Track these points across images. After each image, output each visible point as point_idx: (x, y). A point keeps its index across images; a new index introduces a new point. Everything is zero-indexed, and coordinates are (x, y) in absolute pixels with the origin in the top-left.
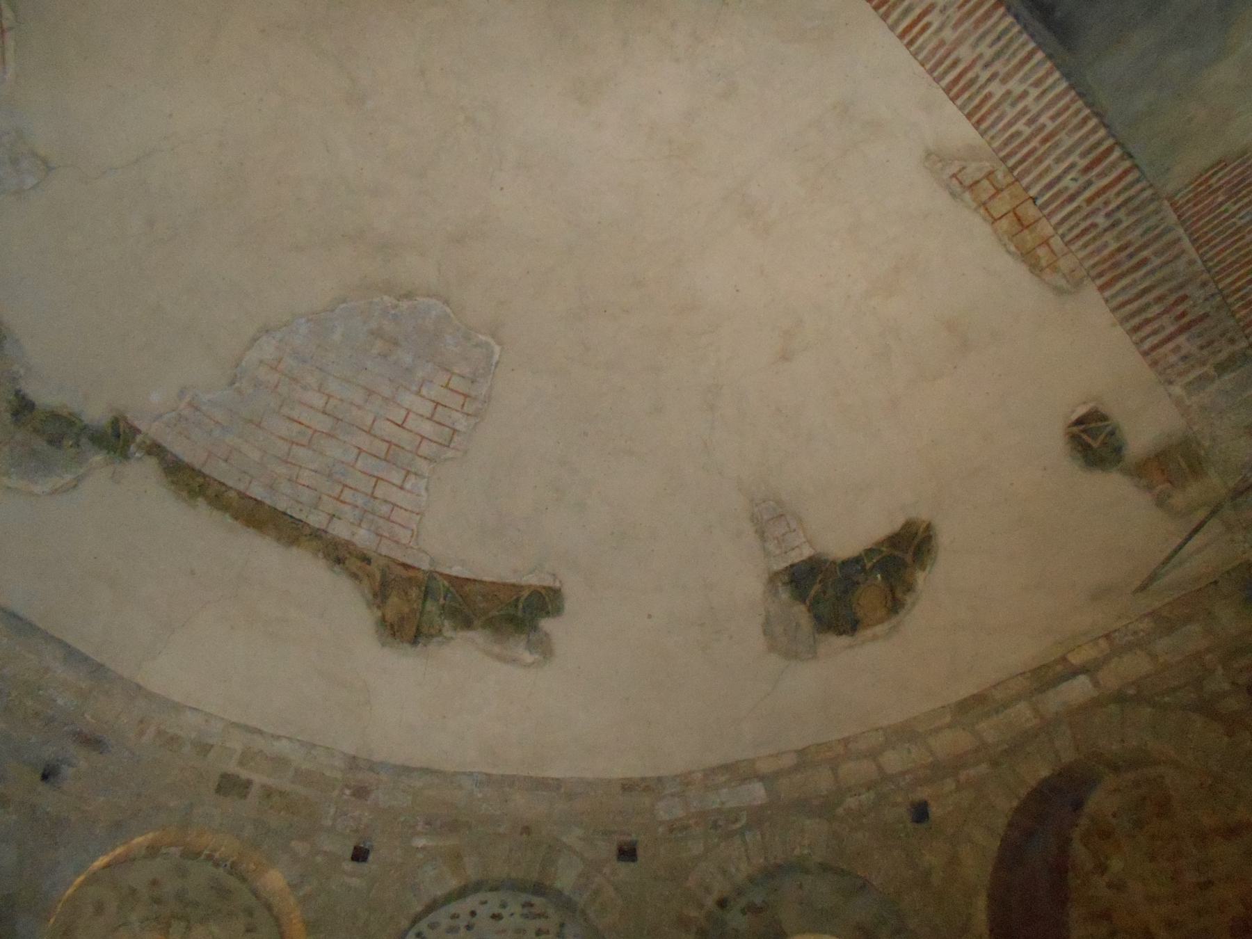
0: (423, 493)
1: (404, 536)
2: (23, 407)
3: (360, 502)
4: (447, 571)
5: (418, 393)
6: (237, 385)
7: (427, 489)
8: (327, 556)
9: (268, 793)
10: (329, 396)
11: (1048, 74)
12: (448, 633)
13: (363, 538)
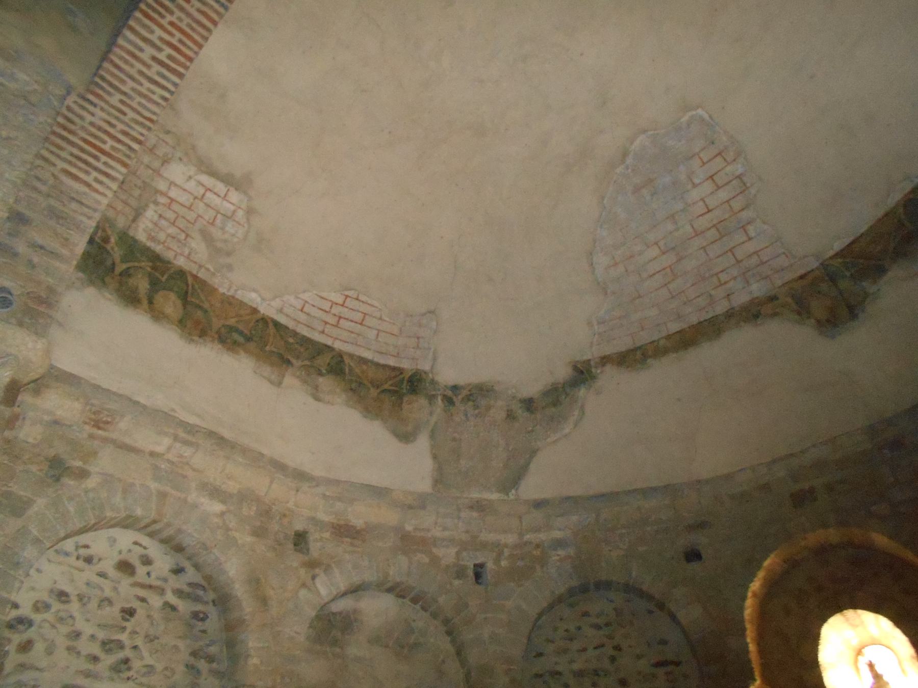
0: (766, 227)
1: (783, 261)
2: (529, 404)
3: (735, 272)
4: (831, 253)
5: (695, 186)
6: (609, 291)
7: (764, 223)
8: (746, 320)
9: (830, 488)
10: (656, 243)
11: (121, 47)
12: (872, 289)
13: (758, 289)
